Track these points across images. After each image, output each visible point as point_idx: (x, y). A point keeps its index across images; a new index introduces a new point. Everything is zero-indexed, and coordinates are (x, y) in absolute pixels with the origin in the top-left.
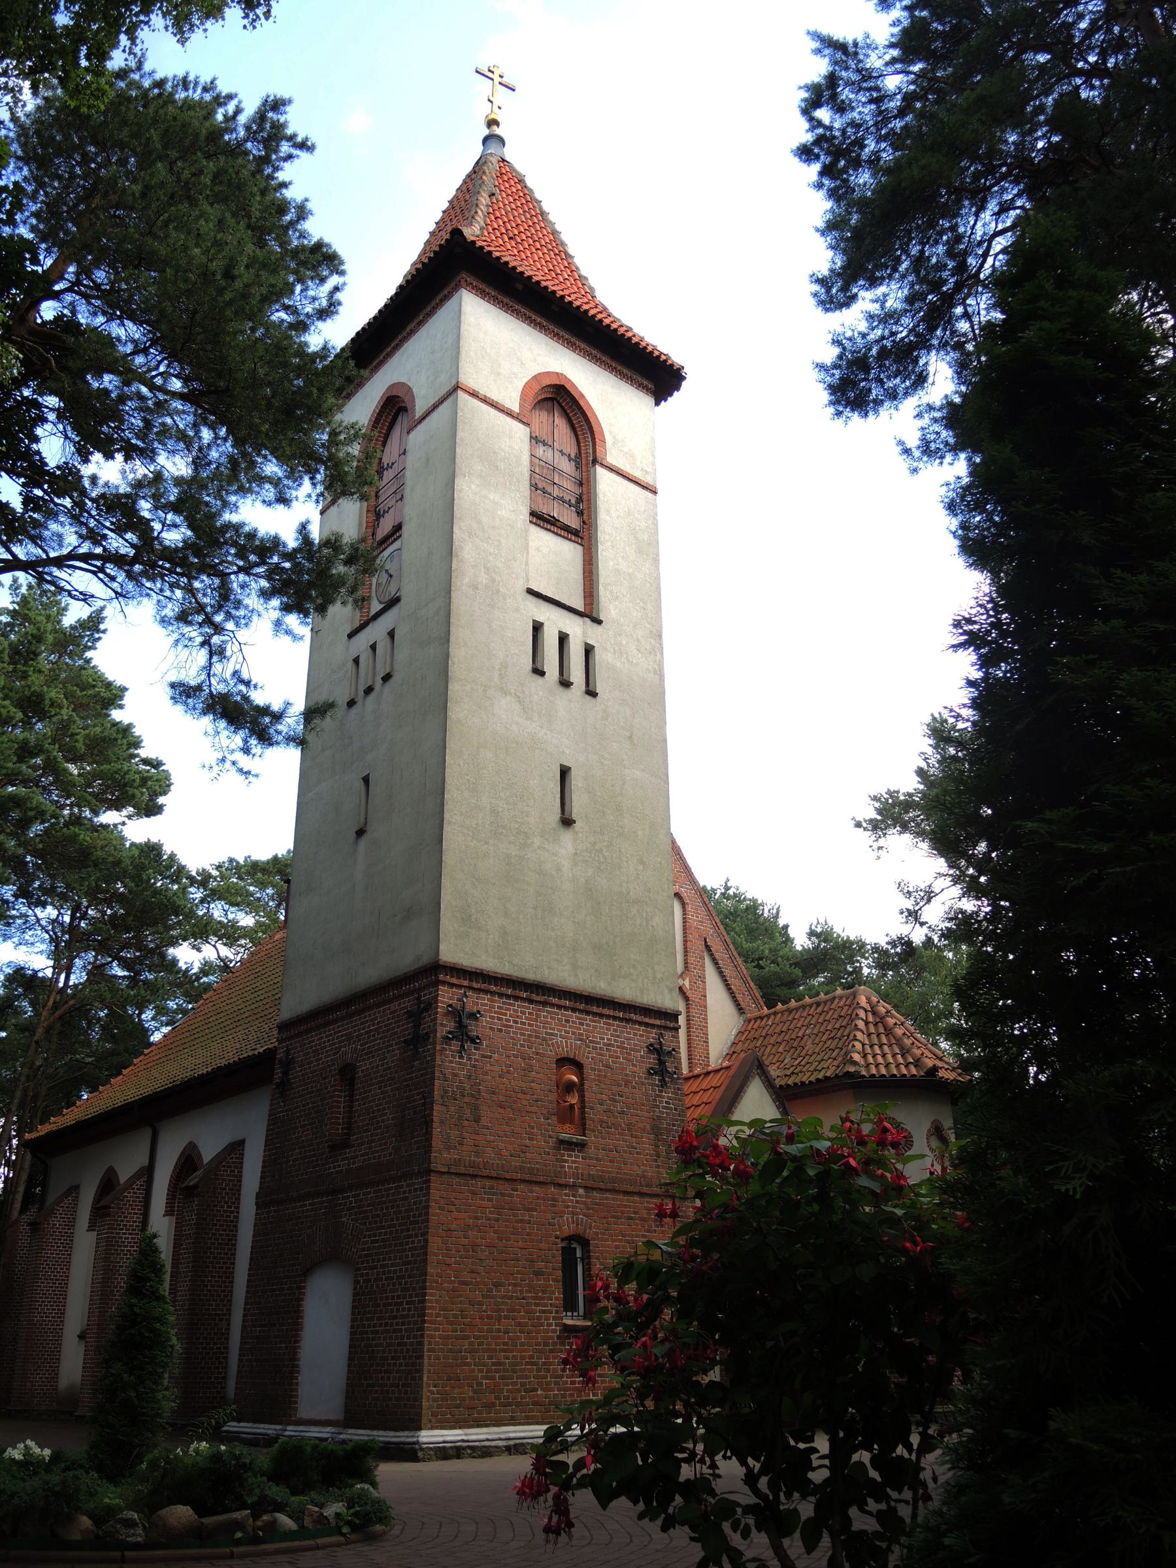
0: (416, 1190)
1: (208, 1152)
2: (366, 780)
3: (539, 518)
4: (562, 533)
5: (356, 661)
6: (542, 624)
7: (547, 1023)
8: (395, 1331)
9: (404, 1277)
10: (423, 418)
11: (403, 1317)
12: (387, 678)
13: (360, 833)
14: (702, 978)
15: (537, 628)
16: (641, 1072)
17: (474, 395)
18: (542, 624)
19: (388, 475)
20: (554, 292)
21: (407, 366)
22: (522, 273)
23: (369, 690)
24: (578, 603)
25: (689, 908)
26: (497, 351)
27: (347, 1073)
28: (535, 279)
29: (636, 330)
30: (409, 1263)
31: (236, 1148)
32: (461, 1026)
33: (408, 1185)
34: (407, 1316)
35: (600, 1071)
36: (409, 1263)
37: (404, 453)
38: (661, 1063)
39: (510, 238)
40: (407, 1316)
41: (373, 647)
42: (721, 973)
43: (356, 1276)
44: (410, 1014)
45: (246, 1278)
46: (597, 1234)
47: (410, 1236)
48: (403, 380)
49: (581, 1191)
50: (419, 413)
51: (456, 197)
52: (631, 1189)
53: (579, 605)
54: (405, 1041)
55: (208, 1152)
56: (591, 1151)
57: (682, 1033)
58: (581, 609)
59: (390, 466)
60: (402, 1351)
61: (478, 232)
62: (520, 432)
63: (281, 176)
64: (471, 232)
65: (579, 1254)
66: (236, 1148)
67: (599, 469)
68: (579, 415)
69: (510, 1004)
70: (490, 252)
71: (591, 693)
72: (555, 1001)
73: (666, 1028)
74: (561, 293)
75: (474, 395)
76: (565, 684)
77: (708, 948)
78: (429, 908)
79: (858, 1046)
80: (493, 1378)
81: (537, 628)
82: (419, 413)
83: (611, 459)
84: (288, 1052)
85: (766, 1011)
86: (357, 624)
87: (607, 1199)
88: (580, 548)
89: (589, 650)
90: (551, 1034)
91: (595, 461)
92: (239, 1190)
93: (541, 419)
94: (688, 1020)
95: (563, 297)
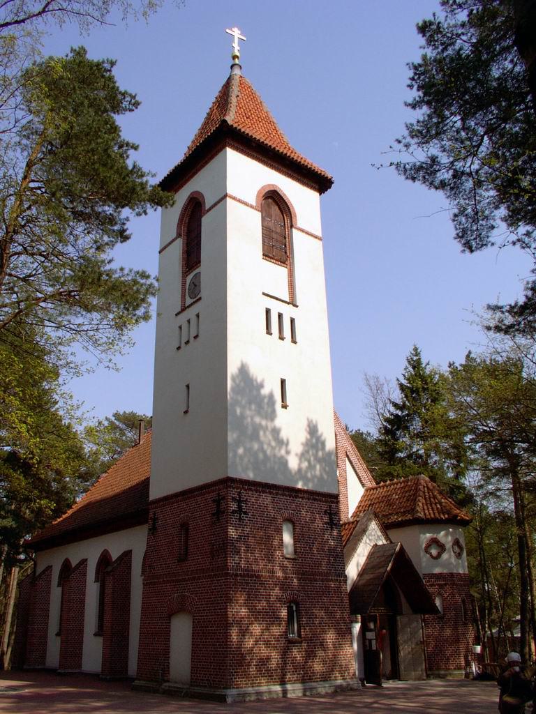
1: (115, 555)
2: (188, 386)
4: (278, 263)
5: (180, 327)
6: (270, 310)
8: (213, 645)
10: (210, 209)
12: (196, 337)
13: (186, 412)
14: (345, 471)
15: (268, 311)
17: (234, 198)
18: (270, 310)
21: (198, 184)
23: (187, 342)
26: (243, 176)
27: (185, 526)
29: (308, 160)
38: (331, 519)
41: (189, 321)
42: (354, 468)
44: (214, 501)
45: (139, 626)
47: (219, 603)
55: (115, 555)
58: (288, 301)
63: (445, 370)
64: (230, 118)
65: (294, 609)
66: (127, 555)
68: (285, 206)
71: (294, 341)
73: (332, 502)
75: (234, 198)
76: (282, 338)
77: (348, 456)
78: (227, 473)
79: (420, 504)
81: (268, 311)
84: (155, 514)
88: (286, 269)
89: (292, 321)
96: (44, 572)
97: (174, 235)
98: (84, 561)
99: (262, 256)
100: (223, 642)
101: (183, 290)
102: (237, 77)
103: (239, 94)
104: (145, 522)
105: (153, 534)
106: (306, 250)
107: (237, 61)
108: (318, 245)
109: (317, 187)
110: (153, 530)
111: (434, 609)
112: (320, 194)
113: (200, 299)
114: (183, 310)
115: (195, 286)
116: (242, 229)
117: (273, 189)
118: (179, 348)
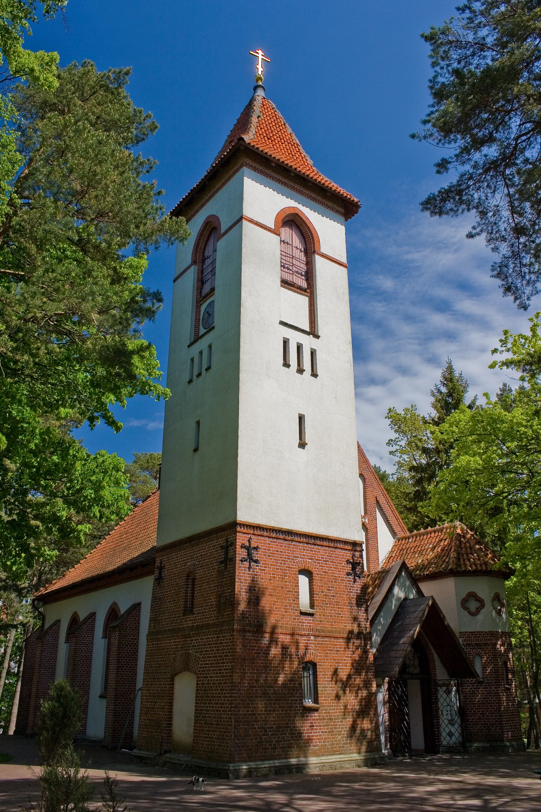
0: (227, 639)
2: (198, 423)
3: (285, 283)
5: (192, 360)
7: (294, 551)
8: (217, 711)
9: (221, 683)
10: (225, 233)
11: (221, 704)
13: (196, 450)
15: (286, 342)
16: (343, 575)
19: (208, 262)
20: (291, 167)
22: (274, 158)
23: (199, 375)
24: (307, 329)
25: (367, 481)
26: (261, 199)
27: (191, 578)
28: (282, 160)
30: (224, 676)
31: (137, 607)
32: (249, 555)
33: (223, 637)
34: (223, 704)
35: (321, 575)
36: (224, 676)
37: (216, 251)
39: (268, 139)
40: (223, 704)
41: (201, 353)
43: (197, 681)
46: (320, 659)
47: (224, 663)
48: (214, 213)
49: (312, 638)
50: (223, 231)
51: (240, 117)
52: (338, 635)
53: (307, 329)
54: (220, 562)
56: (317, 616)
57: (364, 553)
59: (208, 258)
60: (220, 742)
61: (252, 137)
62: (275, 239)
64: (247, 138)
66: (137, 607)
67: (317, 257)
69: (274, 542)
70: (258, 148)
71: (314, 375)
72: (298, 539)
74: (295, 167)
75: (251, 221)
76: (300, 371)
80: (268, 735)
81: (286, 342)
82: (223, 231)
83: (323, 250)
84: (161, 563)
85: (408, 534)
86: (193, 340)
87: (326, 641)
89: (313, 353)
90: (296, 557)
91: (314, 252)
92: (138, 628)
93: (287, 233)
94: (367, 546)
95: (296, 169)
96: (51, 627)
97: (189, 262)
98: (92, 615)
99: (279, 283)
100: (228, 707)
101: (197, 320)
102: (260, 98)
103: (261, 114)
104: (151, 573)
105: (159, 583)
106: (332, 280)
107: (260, 83)
108: (345, 270)
109: (343, 211)
110: (159, 580)
111: (472, 674)
112: (346, 220)
113: (213, 328)
114: (195, 341)
115: (210, 315)
116: (261, 255)
117: (293, 212)
118: (190, 382)
